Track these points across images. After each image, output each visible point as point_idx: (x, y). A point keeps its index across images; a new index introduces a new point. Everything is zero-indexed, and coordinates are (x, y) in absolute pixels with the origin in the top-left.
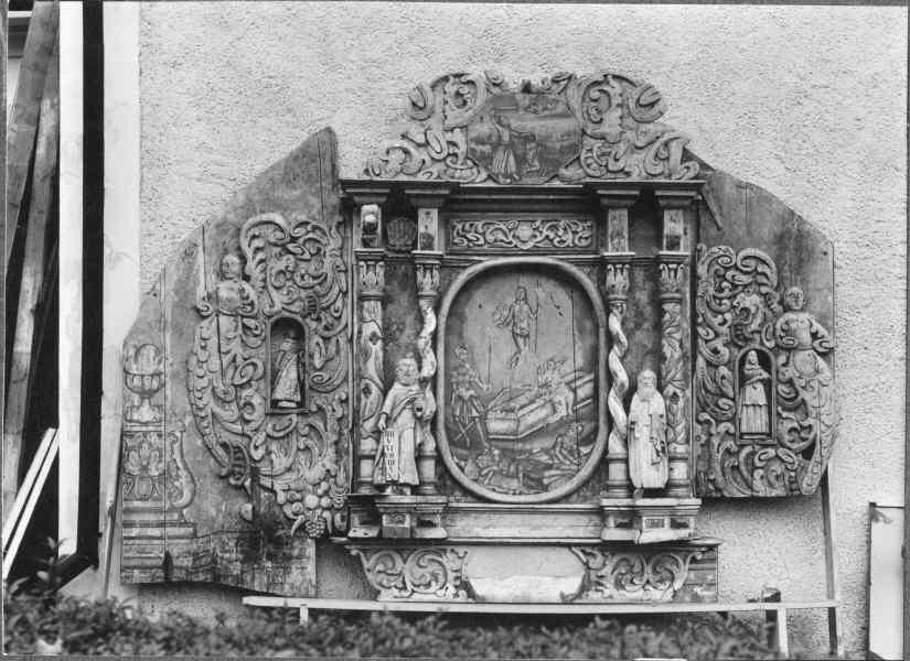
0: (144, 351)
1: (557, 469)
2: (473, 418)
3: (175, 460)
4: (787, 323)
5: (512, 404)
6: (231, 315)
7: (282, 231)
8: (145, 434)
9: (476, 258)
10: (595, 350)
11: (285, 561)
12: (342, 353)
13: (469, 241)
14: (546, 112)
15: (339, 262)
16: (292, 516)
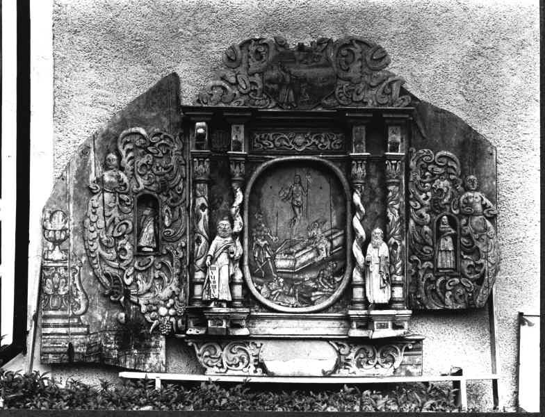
0: (56, 215)
1: (320, 291)
2: (266, 259)
8: (56, 268)
11: (146, 350)
13: (264, 145)
16: (151, 321)
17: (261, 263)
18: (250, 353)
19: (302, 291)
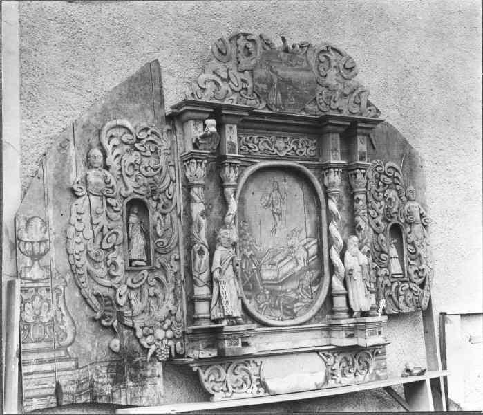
0: (33, 223)
1: (301, 302)
2: (253, 270)
3: (60, 309)
4: (409, 208)
5: (275, 260)
6: (99, 196)
7: (130, 132)
8: (37, 289)
9: (253, 160)
10: (318, 225)
11: (141, 381)
12: (175, 226)
13: (249, 148)
14: (297, 67)
15: (170, 158)
16: (147, 347)
17: (248, 275)
18: (252, 372)
19: (286, 302)
